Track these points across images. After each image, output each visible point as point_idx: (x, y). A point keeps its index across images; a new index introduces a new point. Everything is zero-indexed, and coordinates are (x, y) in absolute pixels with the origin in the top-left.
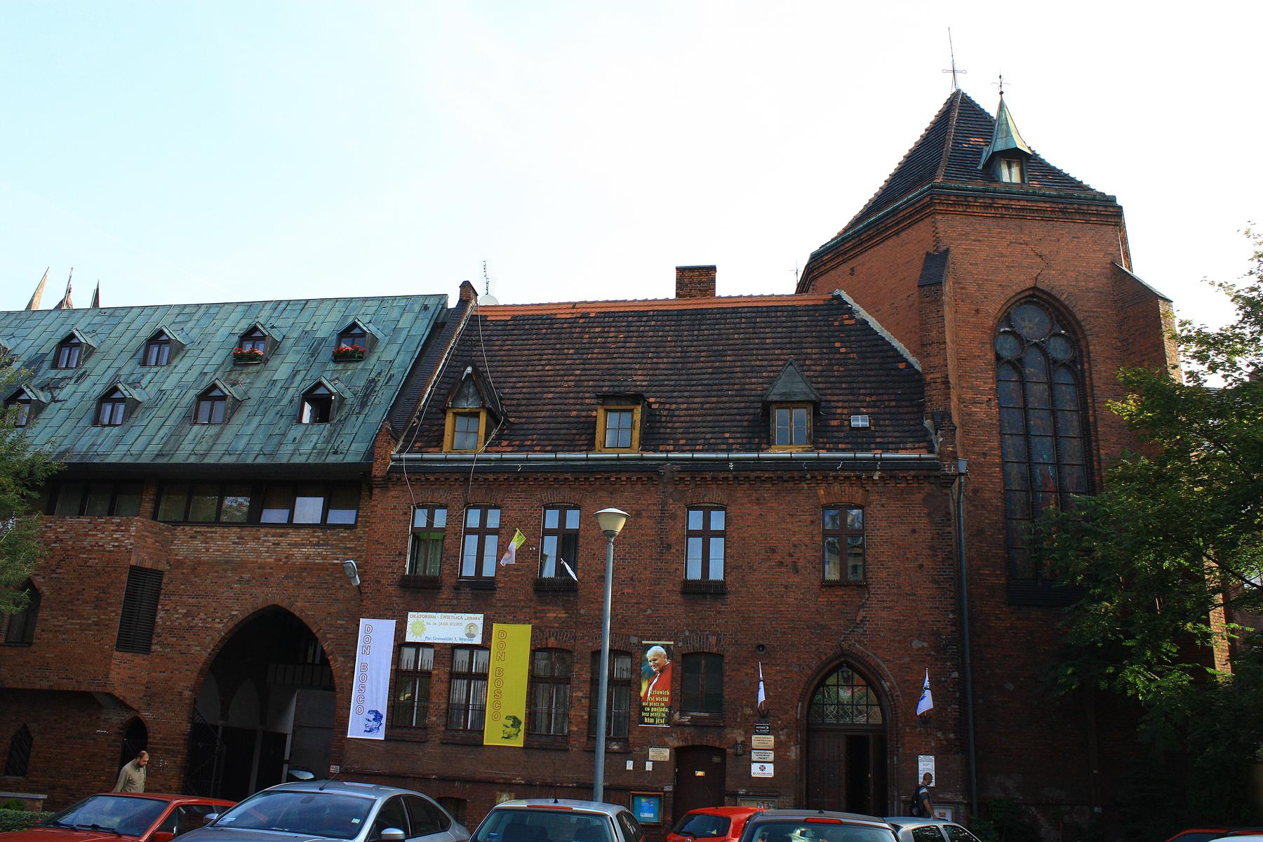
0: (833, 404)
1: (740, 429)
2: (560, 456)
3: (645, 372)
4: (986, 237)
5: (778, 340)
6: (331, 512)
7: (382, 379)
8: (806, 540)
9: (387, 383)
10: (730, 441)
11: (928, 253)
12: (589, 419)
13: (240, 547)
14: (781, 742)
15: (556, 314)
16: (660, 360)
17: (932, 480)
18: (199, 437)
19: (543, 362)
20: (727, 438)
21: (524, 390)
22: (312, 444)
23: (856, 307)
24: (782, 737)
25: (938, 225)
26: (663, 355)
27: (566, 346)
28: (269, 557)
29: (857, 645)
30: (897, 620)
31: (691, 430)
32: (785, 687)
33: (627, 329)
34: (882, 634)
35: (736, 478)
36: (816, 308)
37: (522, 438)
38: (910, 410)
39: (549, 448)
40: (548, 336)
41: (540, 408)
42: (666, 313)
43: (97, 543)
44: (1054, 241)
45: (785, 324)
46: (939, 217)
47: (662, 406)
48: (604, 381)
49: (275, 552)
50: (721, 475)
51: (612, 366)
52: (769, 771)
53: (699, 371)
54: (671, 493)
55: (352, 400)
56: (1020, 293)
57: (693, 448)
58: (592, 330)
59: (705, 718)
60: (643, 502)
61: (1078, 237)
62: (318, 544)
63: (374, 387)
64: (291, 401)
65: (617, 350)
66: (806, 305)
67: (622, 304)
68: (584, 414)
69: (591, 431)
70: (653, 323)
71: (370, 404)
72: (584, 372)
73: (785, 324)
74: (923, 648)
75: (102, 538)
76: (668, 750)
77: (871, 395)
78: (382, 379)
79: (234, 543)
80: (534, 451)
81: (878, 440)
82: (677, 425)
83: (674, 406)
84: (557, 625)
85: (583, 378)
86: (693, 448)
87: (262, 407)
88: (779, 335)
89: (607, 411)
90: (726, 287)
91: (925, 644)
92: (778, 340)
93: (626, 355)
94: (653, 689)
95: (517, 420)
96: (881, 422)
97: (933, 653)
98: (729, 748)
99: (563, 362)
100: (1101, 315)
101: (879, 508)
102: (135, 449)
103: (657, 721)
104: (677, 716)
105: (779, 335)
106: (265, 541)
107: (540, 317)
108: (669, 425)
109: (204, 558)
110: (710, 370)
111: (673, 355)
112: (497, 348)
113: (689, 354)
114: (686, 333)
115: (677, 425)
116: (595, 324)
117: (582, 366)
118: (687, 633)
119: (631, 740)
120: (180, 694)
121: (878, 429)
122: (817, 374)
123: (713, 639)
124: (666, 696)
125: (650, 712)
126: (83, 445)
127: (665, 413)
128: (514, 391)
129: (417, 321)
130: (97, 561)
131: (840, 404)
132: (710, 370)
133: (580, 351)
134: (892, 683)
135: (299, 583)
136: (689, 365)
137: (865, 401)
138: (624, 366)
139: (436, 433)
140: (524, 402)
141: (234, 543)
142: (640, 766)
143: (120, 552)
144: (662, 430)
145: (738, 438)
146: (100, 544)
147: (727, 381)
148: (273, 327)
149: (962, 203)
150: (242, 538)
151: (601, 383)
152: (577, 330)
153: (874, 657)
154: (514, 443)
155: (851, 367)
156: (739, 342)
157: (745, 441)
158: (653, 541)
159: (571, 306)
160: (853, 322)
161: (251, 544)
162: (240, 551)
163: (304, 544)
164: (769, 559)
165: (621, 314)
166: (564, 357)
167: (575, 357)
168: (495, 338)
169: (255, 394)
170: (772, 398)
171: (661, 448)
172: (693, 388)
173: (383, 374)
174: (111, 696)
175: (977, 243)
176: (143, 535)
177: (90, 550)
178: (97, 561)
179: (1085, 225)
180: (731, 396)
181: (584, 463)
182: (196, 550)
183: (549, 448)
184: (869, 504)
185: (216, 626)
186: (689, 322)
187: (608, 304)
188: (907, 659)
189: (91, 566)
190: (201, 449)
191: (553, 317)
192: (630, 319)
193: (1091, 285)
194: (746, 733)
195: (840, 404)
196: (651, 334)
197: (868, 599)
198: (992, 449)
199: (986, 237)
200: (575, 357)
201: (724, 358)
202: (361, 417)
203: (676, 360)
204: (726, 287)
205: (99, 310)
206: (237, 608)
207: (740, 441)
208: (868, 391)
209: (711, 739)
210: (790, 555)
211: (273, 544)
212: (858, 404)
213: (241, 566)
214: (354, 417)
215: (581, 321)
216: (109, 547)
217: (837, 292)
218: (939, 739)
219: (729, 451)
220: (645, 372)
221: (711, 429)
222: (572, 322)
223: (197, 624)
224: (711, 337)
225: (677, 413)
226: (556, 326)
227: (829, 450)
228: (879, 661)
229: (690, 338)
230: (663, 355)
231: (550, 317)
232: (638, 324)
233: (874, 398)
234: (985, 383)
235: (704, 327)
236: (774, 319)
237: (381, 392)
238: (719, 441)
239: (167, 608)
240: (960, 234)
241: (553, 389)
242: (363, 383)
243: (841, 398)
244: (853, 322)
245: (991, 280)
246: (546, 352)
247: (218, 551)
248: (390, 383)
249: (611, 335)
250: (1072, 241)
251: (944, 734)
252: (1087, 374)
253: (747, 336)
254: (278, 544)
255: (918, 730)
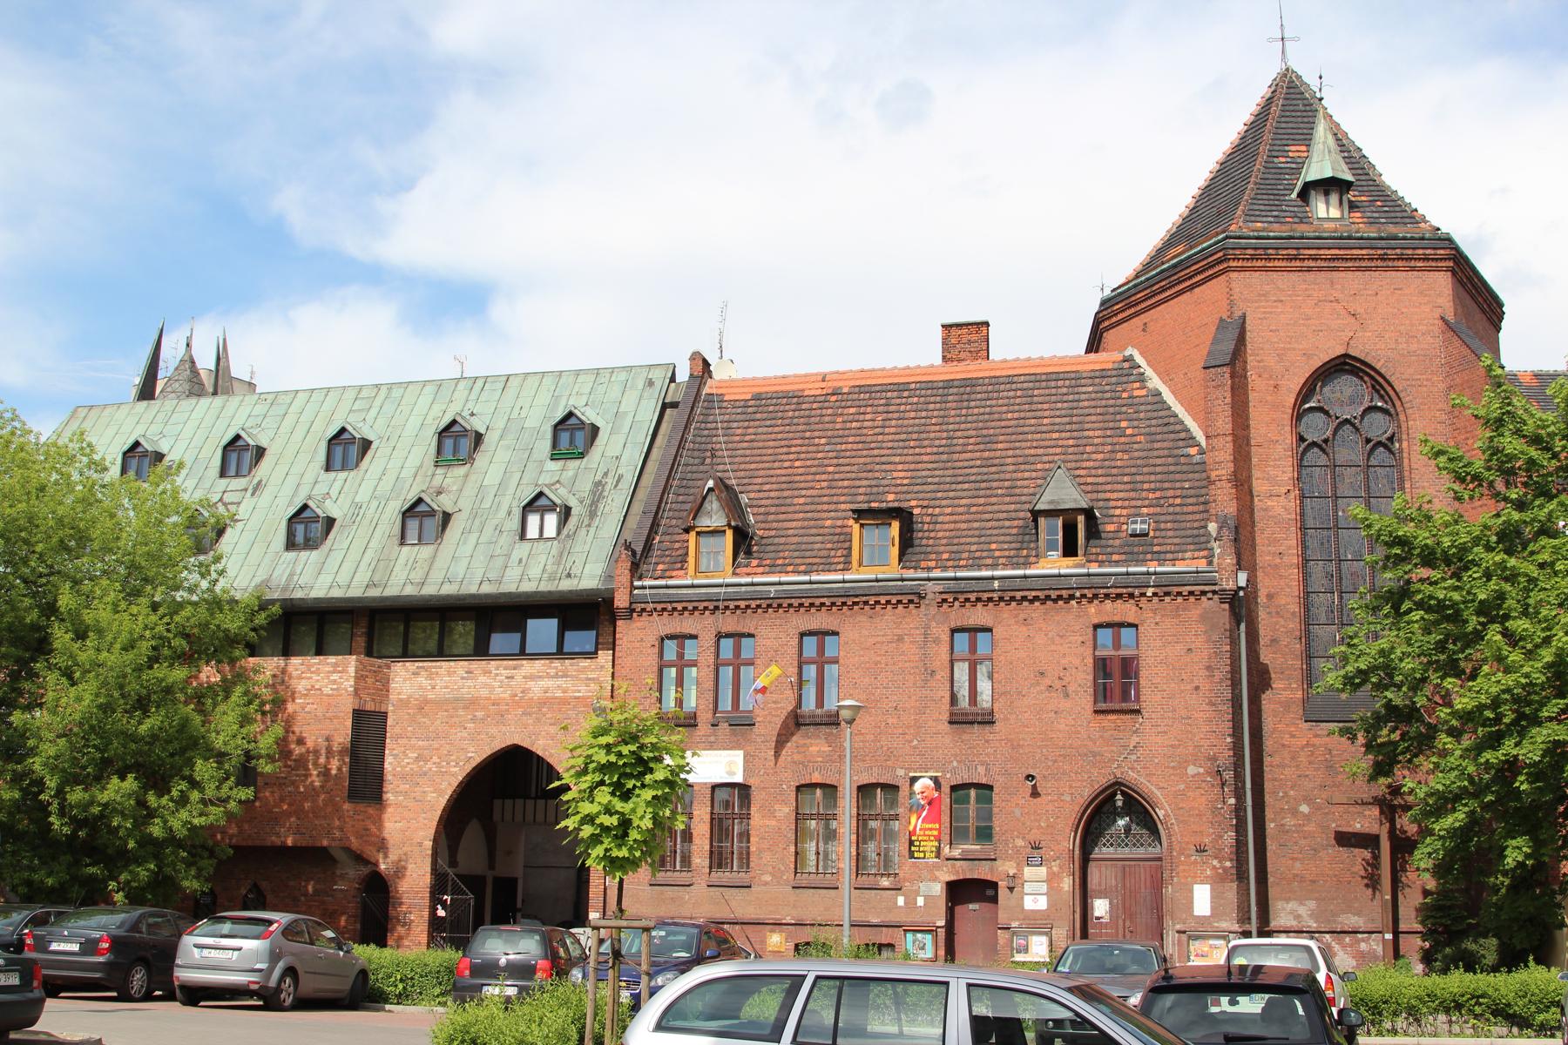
0: (1112, 504)
1: (1008, 538)
2: (815, 577)
3: (906, 467)
4: (1290, 296)
5: (1057, 420)
6: (568, 635)
7: (610, 481)
8: (1077, 662)
9: (616, 486)
10: (997, 554)
11: (1221, 320)
12: (845, 530)
13: (469, 683)
14: (1054, 873)
15: (803, 390)
16: (923, 451)
17: (1210, 595)
18: (412, 560)
19: (792, 457)
20: (994, 550)
21: (772, 494)
22: (541, 566)
23: (1149, 372)
24: (1055, 869)
25: (1233, 285)
26: (926, 443)
27: (817, 434)
28: (504, 692)
29: (1130, 773)
30: (1172, 746)
31: (956, 541)
32: (1058, 817)
33: (885, 409)
34: (1156, 761)
35: (1001, 599)
36: (1103, 374)
37: (772, 555)
38: (1195, 508)
39: (802, 568)
40: (795, 421)
41: (790, 516)
42: (930, 385)
43: (313, 686)
44: (1370, 295)
45: (1065, 398)
46: (1234, 275)
47: (925, 511)
48: (860, 479)
49: (510, 686)
50: (985, 596)
51: (868, 460)
52: (1042, 904)
53: (966, 464)
54: (934, 615)
55: (578, 508)
56: (1328, 362)
57: (956, 563)
58: (846, 411)
59: (976, 851)
60: (906, 626)
61: (1400, 289)
62: (556, 676)
63: (602, 491)
64: (509, 513)
65: (874, 438)
66: (1092, 371)
67: (879, 373)
68: (839, 523)
69: (847, 545)
70: (915, 400)
71: (599, 514)
72: (837, 469)
73: (1065, 398)
74: (1199, 774)
75: (318, 680)
76: (939, 885)
77: (1155, 490)
78: (610, 481)
79: (463, 678)
80: (787, 572)
81: (1156, 549)
82: (940, 534)
83: (937, 511)
84: (820, 759)
85: (837, 476)
86: (956, 563)
87: (477, 522)
88: (1058, 413)
89: (862, 526)
90: (1006, 348)
91: (1201, 770)
92: (1057, 420)
93: (884, 445)
94: (923, 822)
95: (767, 533)
96: (1162, 526)
97: (1209, 779)
98: (1001, 880)
99: (814, 455)
100: (1425, 383)
101: (1153, 626)
102: (343, 578)
103: (927, 855)
104: (946, 850)
105: (1058, 413)
106: (497, 675)
107: (786, 396)
108: (932, 535)
109: (431, 696)
110: (979, 463)
111: (937, 443)
112: (737, 438)
113: (955, 441)
114: (953, 413)
115: (940, 534)
116: (849, 403)
117: (835, 461)
118: (955, 764)
119: (901, 875)
120: (420, 844)
121: (1158, 534)
122: (1097, 464)
123: (981, 769)
124: (935, 829)
125: (919, 846)
126: (280, 576)
127: (928, 519)
128: (761, 495)
129: (642, 401)
130: (315, 706)
131: (1119, 503)
132: (979, 463)
133: (833, 441)
134: (1166, 810)
135: (538, 720)
136: (956, 456)
137: (1147, 499)
138: (883, 459)
139: (679, 552)
140: (773, 510)
141: (463, 678)
142: (911, 903)
143: (341, 695)
144: (924, 542)
145: (1005, 550)
146: (317, 687)
147: (996, 476)
148: (472, 414)
149: (1262, 256)
150: (471, 673)
151: (858, 483)
152: (830, 411)
153: (1148, 784)
154: (765, 563)
155: (1136, 454)
156: (1013, 423)
157: (1012, 553)
158: (917, 667)
159: (820, 378)
160: (1143, 392)
161: (482, 679)
162: (469, 687)
163: (540, 677)
164: (1038, 684)
165: (878, 388)
166: (814, 449)
167: (827, 448)
168: (735, 425)
169: (465, 503)
170: (1040, 507)
171: (923, 564)
172: (960, 486)
173: (609, 475)
174: (348, 850)
175: (1280, 304)
176: (362, 676)
177: (307, 695)
178: (315, 706)
179: (1410, 273)
180: (1002, 495)
181: (840, 585)
182: (421, 687)
183: (802, 568)
184: (1143, 622)
185: (452, 769)
186: (956, 398)
187: (863, 374)
188: (1182, 787)
189: (309, 713)
190: (417, 576)
191: (800, 394)
192: (889, 394)
193: (1414, 347)
194: (1018, 864)
195: (1119, 503)
196: (913, 414)
197: (1141, 724)
198: (1289, 548)
199: (1290, 296)
200: (827, 448)
201: (995, 446)
202: (592, 530)
203: (941, 449)
204: (1006, 348)
205: (257, 397)
206: (473, 749)
207: (1007, 553)
208: (1153, 486)
209: (981, 872)
210: (1060, 678)
211: (507, 678)
212: (1139, 503)
213: (472, 703)
214: (583, 531)
215: (833, 398)
216: (327, 691)
217: (1129, 351)
218: (1214, 868)
219: (994, 566)
220: (906, 467)
221: (976, 539)
222: (823, 400)
223: (430, 769)
224: (981, 418)
225: (940, 519)
226: (804, 406)
227: (1101, 563)
228: (1153, 788)
229: (958, 419)
230: (926, 443)
231: (796, 394)
232: (898, 401)
233: (1158, 494)
234: (1284, 472)
235: (973, 404)
236: (1054, 391)
237: (610, 498)
238: (985, 554)
239: (395, 752)
240: (1260, 295)
241: (804, 492)
242: (588, 486)
243: (1121, 495)
244: (1143, 392)
245: (1294, 349)
246: (795, 442)
247: (446, 687)
248: (620, 486)
249: (868, 417)
250: (1393, 293)
251: (1220, 862)
252: (1405, 455)
253: (1022, 415)
254: (513, 678)
255: (1193, 858)
